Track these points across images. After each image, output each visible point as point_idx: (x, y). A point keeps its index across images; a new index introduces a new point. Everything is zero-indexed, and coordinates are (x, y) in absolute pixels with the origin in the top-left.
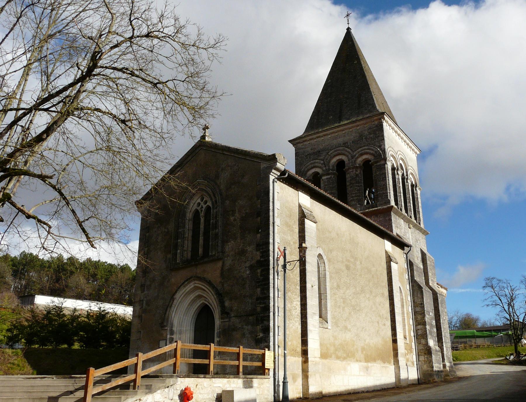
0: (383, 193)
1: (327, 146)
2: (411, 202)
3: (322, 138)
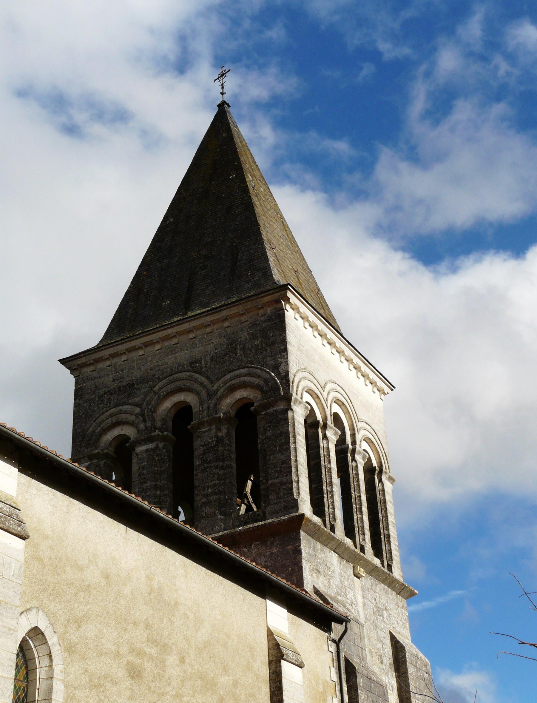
0: (282, 484)
1: (151, 370)
2: (365, 509)
3: (141, 352)
